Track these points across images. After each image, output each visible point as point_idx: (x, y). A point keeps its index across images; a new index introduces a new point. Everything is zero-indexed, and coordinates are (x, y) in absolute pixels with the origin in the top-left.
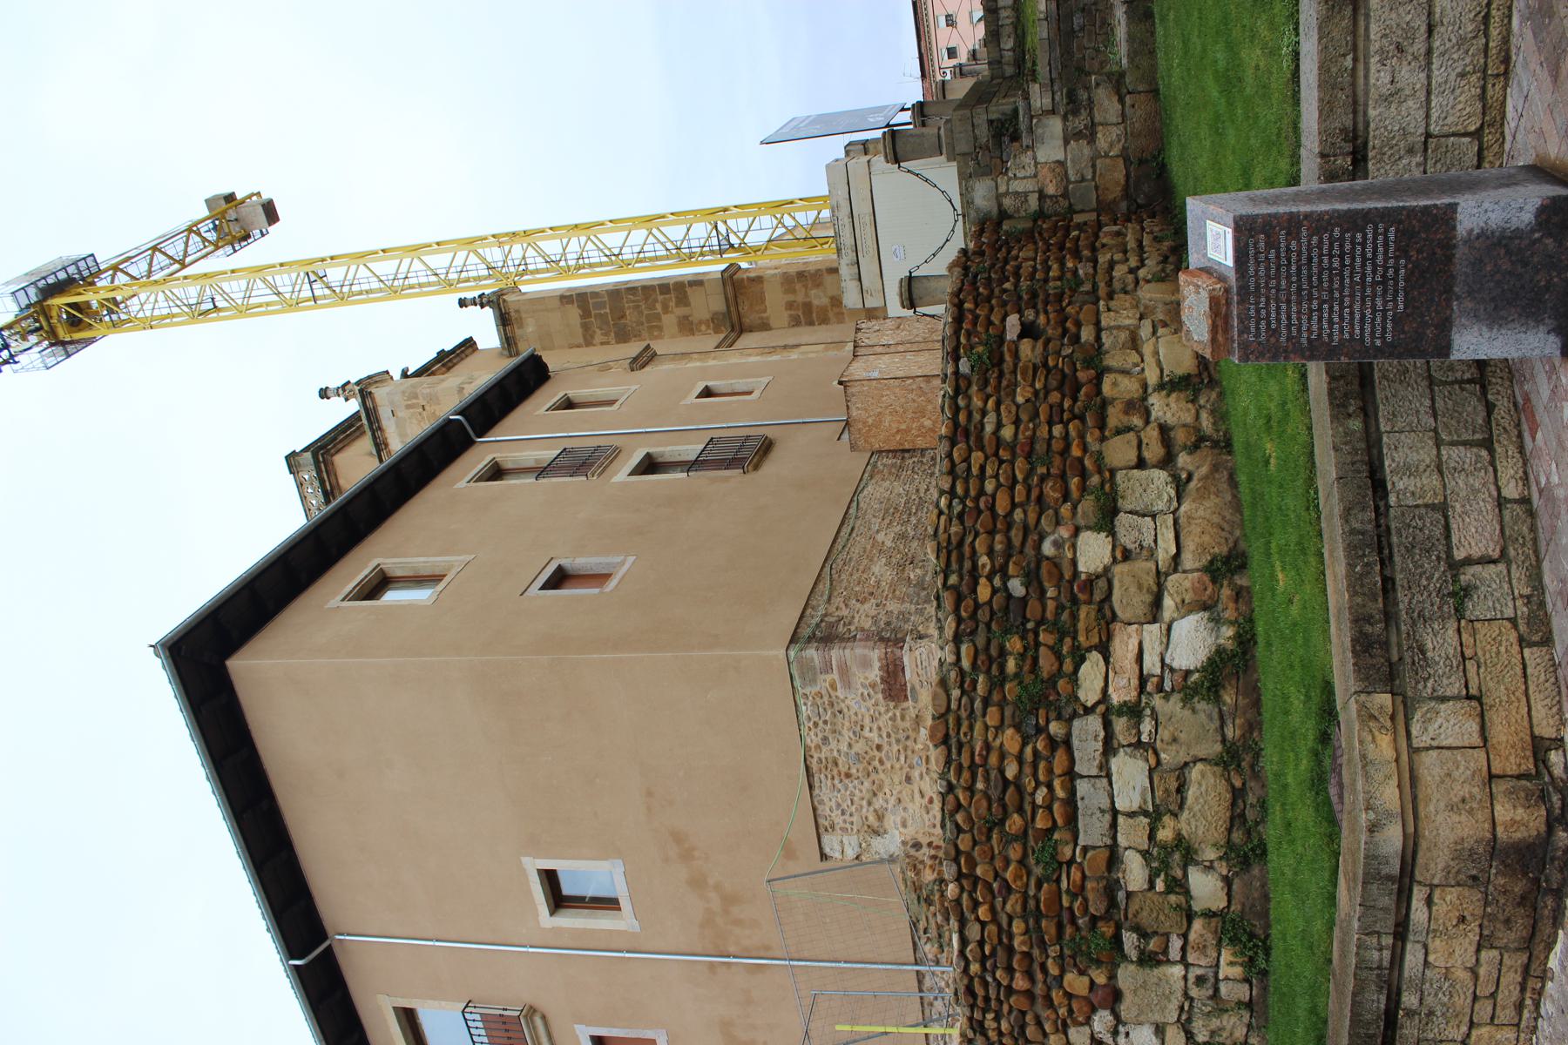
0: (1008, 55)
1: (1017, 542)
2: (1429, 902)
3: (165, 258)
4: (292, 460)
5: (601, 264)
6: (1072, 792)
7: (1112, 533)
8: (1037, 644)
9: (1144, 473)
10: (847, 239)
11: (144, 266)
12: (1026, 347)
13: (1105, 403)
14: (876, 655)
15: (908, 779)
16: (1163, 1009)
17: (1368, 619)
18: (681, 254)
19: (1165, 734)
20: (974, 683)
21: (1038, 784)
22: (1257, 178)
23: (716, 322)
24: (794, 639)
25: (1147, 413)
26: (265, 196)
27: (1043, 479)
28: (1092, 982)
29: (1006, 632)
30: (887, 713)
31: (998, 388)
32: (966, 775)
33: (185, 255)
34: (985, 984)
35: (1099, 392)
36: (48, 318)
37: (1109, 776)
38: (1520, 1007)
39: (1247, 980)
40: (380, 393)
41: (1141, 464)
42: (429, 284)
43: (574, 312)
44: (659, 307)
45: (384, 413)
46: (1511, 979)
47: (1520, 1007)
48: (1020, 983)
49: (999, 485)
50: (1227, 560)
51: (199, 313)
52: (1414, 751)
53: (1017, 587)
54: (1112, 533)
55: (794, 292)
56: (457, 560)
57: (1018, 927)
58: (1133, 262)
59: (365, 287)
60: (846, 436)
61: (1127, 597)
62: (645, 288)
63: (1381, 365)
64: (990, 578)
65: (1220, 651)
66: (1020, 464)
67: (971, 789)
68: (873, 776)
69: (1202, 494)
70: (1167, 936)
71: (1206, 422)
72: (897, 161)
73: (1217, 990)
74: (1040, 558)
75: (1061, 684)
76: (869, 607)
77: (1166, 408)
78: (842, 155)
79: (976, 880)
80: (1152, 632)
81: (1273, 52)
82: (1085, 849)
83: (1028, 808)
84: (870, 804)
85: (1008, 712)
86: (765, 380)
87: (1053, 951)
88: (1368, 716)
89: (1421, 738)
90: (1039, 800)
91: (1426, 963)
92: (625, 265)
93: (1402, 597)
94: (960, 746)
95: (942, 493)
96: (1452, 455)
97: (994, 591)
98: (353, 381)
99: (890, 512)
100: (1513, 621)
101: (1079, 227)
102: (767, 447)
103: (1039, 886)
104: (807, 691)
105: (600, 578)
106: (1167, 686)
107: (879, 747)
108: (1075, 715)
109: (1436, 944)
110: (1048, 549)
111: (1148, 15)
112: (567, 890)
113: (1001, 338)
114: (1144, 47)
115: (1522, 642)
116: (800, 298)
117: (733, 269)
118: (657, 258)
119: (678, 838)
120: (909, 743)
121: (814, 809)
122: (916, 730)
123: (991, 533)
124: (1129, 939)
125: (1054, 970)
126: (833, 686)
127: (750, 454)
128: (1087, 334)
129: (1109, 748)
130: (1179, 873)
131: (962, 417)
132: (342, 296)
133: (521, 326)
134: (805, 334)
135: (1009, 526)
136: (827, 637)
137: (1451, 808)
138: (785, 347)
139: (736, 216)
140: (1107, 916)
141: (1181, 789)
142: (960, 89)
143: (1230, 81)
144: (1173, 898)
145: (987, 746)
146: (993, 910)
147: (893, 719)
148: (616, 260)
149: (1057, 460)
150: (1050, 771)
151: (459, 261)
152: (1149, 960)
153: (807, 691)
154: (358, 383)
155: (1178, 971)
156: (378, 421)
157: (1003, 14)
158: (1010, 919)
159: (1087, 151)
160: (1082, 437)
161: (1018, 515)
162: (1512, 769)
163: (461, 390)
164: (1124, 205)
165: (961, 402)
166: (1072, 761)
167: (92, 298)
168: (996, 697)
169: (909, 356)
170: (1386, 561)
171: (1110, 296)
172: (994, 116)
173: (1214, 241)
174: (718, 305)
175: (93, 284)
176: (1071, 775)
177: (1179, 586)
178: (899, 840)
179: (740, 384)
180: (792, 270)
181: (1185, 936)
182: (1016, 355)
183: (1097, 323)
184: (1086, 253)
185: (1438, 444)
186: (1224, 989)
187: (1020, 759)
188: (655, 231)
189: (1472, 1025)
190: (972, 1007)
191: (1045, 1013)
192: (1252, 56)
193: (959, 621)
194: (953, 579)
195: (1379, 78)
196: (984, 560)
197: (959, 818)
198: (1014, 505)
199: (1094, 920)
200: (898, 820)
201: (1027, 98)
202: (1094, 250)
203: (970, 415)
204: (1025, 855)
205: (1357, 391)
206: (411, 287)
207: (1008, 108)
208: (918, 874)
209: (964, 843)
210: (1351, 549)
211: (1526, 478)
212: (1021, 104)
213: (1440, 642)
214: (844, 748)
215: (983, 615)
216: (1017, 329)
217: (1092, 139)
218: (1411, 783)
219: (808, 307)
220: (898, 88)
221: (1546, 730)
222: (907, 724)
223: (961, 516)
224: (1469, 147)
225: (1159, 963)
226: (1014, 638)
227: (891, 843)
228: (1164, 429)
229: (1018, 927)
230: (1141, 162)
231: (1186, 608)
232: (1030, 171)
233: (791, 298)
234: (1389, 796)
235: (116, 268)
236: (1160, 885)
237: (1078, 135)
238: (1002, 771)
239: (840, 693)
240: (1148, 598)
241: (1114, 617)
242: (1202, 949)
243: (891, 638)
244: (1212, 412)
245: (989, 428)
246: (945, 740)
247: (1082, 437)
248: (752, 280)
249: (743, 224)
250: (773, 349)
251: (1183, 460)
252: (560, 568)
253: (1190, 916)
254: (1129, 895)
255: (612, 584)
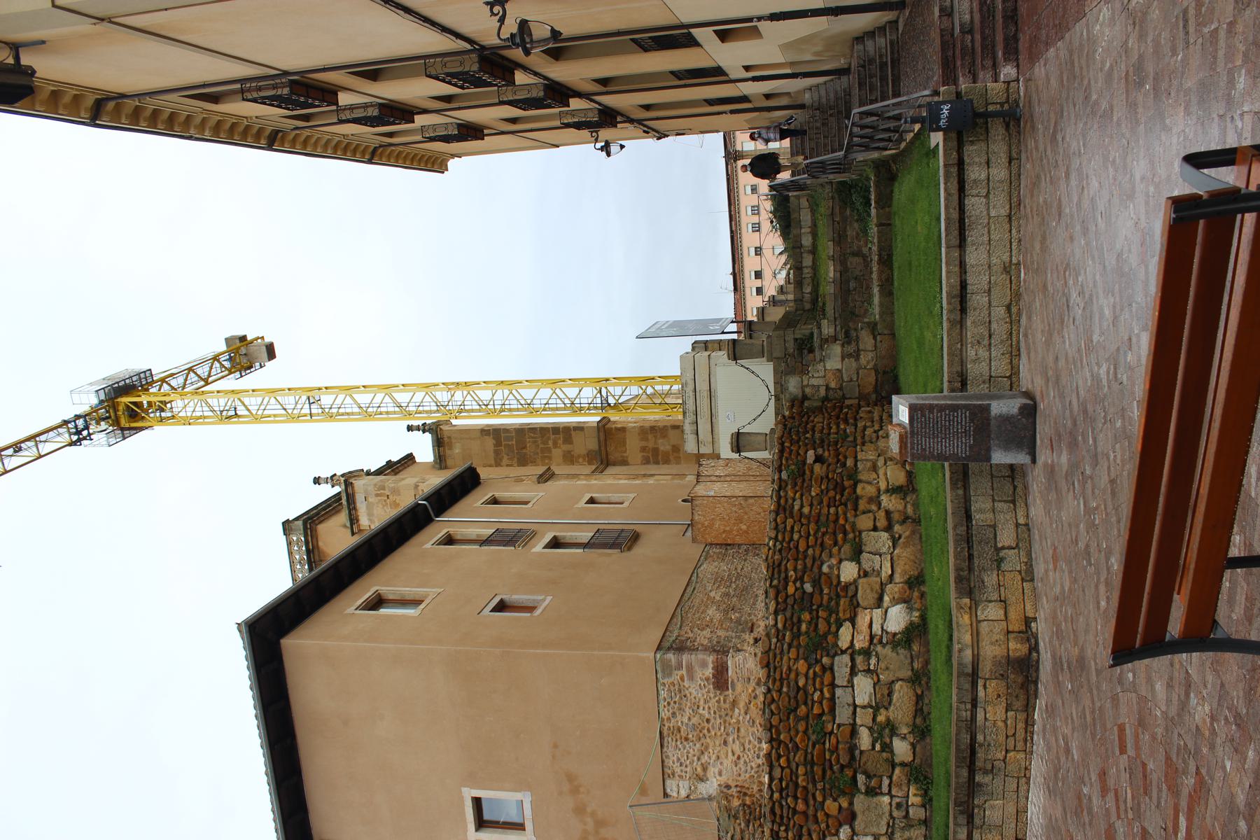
0: (807, 297)
1: (809, 565)
2: (985, 687)
3: (196, 377)
4: (287, 526)
5: (518, 410)
6: (833, 694)
7: (859, 562)
8: (818, 617)
9: (876, 534)
10: (690, 406)
11: (181, 380)
12: (817, 467)
13: (857, 498)
14: (710, 659)
15: (725, 743)
16: (878, 825)
17: (962, 570)
18: (574, 408)
19: (882, 665)
20: (784, 635)
21: (815, 690)
22: (929, 389)
23: (590, 457)
24: (659, 648)
25: (880, 504)
26: (267, 340)
27: (824, 534)
28: (840, 806)
29: (802, 610)
30: (714, 697)
31: (802, 487)
32: (778, 683)
33: (209, 376)
34: (781, 807)
35: (855, 492)
36: (116, 411)
37: (853, 686)
38: (1025, 741)
39: (924, 806)
40: (359, 484)
41: (875, 529)
42: (395, 413)
43: (490, 442)
44: (550, 443)
45: (359, 498)
46: (1021, 725)
47: (1025, 741)
48: (801, 806)
49: (801, 536)
50: (917, 578)
51: (230, 417)
52: (979, 622)
53: (808, 587)
54: (859, 562)
55: (647, 440)
56: (431, 591)
57: (801, 770)
58: (876, 427)
59: (349, 410)
60: (689, 534)
61: (865, 594)
62: (542, 429)
63: (971, 465)
64: (794, 582)
65: (912, 623)
66: (812, 526)
67: (780, 691)
68: (703, 740)
69: (906, 545)
70: (881, 777)
71: (910, 510)
72: (735, 359)
73: (907, 812)
74: (821, 573)
75: (830, 637)
76: (707, 633)
77: (887, 502)
78: (689, 349)
79: (780, 742)
80: (878, 613)
81: (935, 336)
82: (839, 726)
83: (810, 703)
84: (699, 759)
85: (801, 651)
86: (632, 496)
87: (820, 785)
88: (960, 607)
89: (981, 617)
90: (816, 698)
91: (986, 719)
92: (534, 412)
93: (976, 561)
94: (775, 668)
95: (770, 539)
96: (999, 505)
97: (797, 589)
98: (339, 474)
99: (718, 580)
100: (1020, 572)
101: (849, 407)
102: (635, 537)
103: (814, 746)
104: (665, 681)
105: (530, 609)
106: (884, 641)
107: (708, 721)
108: (836, 654)
109: (989, 708)
110: (825, 569)
111: (891, 294)
112: (486, 816)
113: (804, 462)
114: (888, 310)
115: (1023, 580)
116: (651, 445)
117: (604, 423)
118: (557, 409)
119: (571, 778)
120: (728, 718)
121: (663, 762)
122: (732, 710)
123: (796, 560)
124: (861, 778)
125: (819, 798)
126: (682, 679)
127: (624, 540)
128: (850, 463)
129: (853, 672)
130: (888, 740)
131: (782, 501)
132: (329, 416)
133: (451, 448)
134: (652, 469)
135: (805, 557)
136: (681, 647)
137: (992, 644)
138: (644, 476)
139: (614, 385)
140: (849, 765)
141: (890, 694)
142: (776, 314)
143: (921, 343)
144: (884, 754)
145: (789, 669)
146: (788, 760)
147: (718, 702)
148: (529, 408)
149: (832, 525)
150: (822, 683)
151: (339, 401)
152: (872, 792)
153: (665, 681)
154: (343, 475)
155: (886, 799)
156: (354, 503)
157: (806, 271)
158: (797, 766)
159: (854, 365)
160: (845, 514)
161: (810, 551)
162: (1016, 629)
163: (416, 486)
164: (874, 396)
165: (782, 494)
166: (834, 678)
167: (144, 399)
168: (795, 643)
169: (733, 484)
170: (970, 548)
171: (863, 444)
172: (798, 336)
173: (902, 413)
174: (592, 444)
175: (147, 390)
176: (833, 685)
177: (892, 590)
178: (716, 784)
179: (615, 497)
180: (647, 425)
181: (890, 777)
182: (812, 471)
183: (856, 457)
184: (851, 421)
185: (994, 501)
186: (911, 811)
187: (806, 676)
188: (558, 391)
189: (1007, 751)
190: (773, 822)
191: (813, 827)
192: (928, 335)
193: (778, 603)
194: (775, 582)
195: (971, 353)
196: (792, 573)
197: (773, 707)
198: (808, 547)
199: (842, 767)
200: (717, 771)
201: (819, 327)
202: (856, 419)
203: (786, 501)
204: (807, 729)
205: (962, 477)
206: (381, 413)
207: (807, 332)
208: (729, 802)
209: (775, 721)
210: (956, 542)
211: (1027, 516)
212: (816, 331)
213: (990, 579)
214: (685, 720)
215: (790, 601)
216: (813, 458)
217: (857, 358)
218: (976, 635)
219: (656, 451)
220: (717, 306)
221: (1030, 615)
222: (727, 706)
223: (780, 551)
224: (1007, 382)
225: (877, 794)
226: (807, 615)
227: (711, 787)
228: (888, 513)
229: (801, 770)
230: (885, 373)
231: (895, 602)
232: (822, 374)
233: (644, 444)
234: (967, 638)
235: (163, 380)
236: (878, 747)
237: (850, 356)
238: (797, 683)
239: (686, 684)
240: (876, 596)
241: (858, 605)
242: (900, 786)
243: (721, 650)
244: (913, 505)
245: (796, 508)
246: (768, 665)
247: (845, 514)
248: (617, 429)
249: (618, 390)
250: (636, 477)
251: (897, 528)
252: (502, 601)
253: (893, 766)
254: (862, 752)
255: (538, 612)
